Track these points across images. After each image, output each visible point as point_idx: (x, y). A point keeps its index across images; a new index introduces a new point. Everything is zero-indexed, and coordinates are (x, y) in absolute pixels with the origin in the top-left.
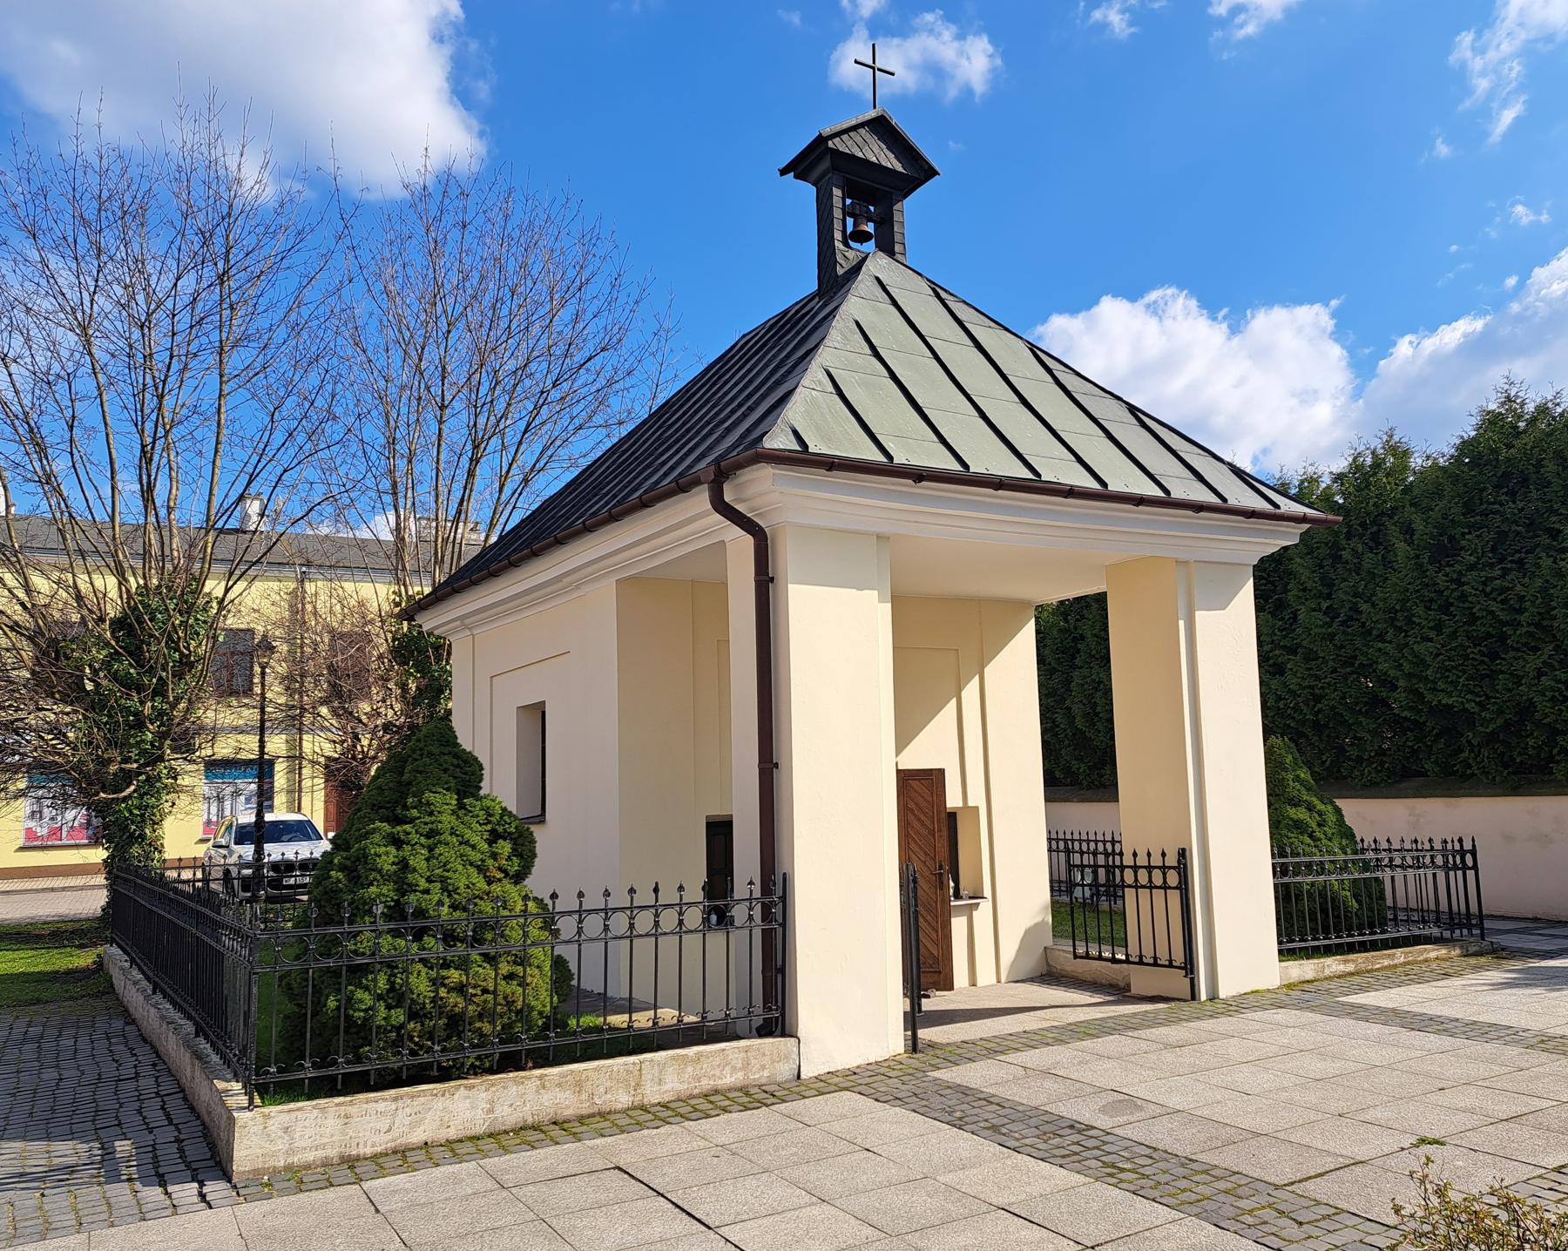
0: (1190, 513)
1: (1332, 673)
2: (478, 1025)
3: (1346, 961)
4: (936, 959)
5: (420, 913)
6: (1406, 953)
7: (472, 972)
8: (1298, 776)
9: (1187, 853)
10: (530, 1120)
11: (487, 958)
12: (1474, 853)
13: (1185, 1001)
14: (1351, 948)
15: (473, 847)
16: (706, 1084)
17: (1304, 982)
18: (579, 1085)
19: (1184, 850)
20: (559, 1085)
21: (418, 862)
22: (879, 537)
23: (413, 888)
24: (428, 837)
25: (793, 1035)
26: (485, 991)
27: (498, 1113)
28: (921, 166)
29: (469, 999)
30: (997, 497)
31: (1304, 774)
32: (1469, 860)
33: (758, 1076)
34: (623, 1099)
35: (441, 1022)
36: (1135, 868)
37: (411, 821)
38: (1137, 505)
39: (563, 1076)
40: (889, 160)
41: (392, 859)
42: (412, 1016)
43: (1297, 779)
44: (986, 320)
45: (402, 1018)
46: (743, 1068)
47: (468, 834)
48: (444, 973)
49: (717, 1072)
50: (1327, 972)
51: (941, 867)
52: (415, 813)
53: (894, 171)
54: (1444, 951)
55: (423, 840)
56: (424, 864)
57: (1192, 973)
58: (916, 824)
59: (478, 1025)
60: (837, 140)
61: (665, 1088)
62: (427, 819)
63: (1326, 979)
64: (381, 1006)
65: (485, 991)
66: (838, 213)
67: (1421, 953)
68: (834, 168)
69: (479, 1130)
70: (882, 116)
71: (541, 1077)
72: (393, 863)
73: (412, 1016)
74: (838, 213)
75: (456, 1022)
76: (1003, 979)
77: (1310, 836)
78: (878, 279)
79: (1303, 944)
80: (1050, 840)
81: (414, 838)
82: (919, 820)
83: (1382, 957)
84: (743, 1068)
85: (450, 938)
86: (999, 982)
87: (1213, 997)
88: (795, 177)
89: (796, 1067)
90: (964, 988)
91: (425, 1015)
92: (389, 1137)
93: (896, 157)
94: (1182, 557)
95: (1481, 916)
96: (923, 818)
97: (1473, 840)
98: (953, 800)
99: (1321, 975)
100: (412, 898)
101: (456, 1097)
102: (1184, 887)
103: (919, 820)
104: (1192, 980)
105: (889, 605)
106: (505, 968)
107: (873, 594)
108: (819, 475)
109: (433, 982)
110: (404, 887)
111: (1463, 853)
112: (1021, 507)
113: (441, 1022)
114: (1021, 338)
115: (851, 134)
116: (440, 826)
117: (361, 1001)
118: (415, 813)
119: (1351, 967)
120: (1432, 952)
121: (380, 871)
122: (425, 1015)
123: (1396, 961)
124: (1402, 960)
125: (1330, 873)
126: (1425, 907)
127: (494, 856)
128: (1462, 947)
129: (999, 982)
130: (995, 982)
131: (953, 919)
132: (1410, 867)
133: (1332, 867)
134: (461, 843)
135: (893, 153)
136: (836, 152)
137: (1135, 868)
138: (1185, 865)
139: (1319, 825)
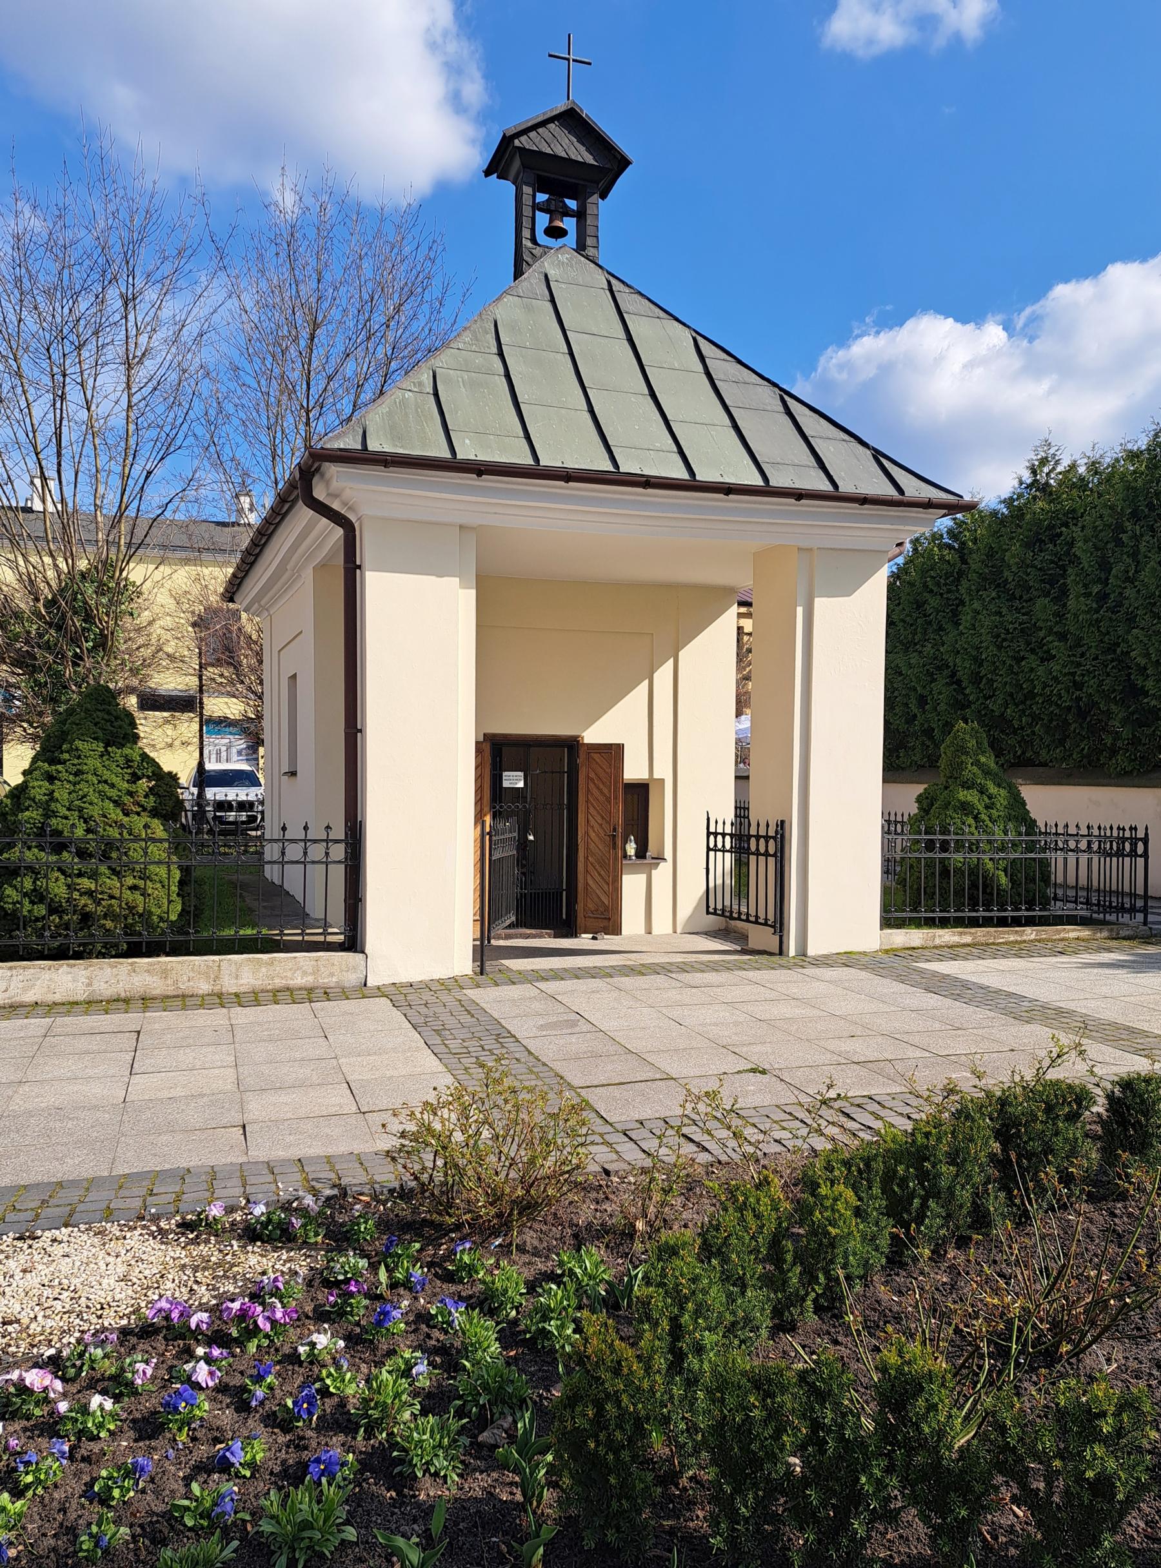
0: (721, 496)
1: (1094, 659)
2: (102, 922)
3: (961, 934)
4: (607, 909)
5: (58, 833)
6: (1038, 931)
7: (100, 882)
8: (979, 761)
9: (787, 825)
10: (123, 995)
11: (114, 872)
12: (1145, 840)
13: (771, 954)
14: (974, 923)
15: (113, 786)
16: (279, 983)
17: (908, 949)
18: (165, 973)
19: (783, 822)
20: (148, 971)
21: (62, 793)
22: (461, 527)
23: (54, 814)
24: (76, 775)
25: (363, 952)
26: (112, 897)
27: (95, 987)
28: (615, 156)
29: (98, 903)
30: (567, 488)
31: (985, 759)
32: (1140, 848)
33: (325, 980)
34: (204, 987)
35: (75, 918)
36: (758, 837)
37: (64, 762)
38: (727, 494)
39: (150, 964)
40: (579, 153)
41: (43, 791)
42: (52, 910)
43: (977, 763)
44: (657, 310)
45: (44, 912)
46: (314, 973)
47: (107, 775)
48: (79, 881)
49: (289, 974)
50: (937, 942)
51: (615, 830)
52: (66, 756)
53: (584, 164)
54: (1087, 933)
55: (71, 778)
56: (66, 796)
57: (781, 931)
58: (595, 791)
59: (102, 922)
60: (524, 138)
61: (242, 982)
62: (76, 761)
63: (935, 947)
64: (26, 902)
65: (112, 897)
66: (527, 211)
67: (1059, 932)
68: (524, 166)
69: (81, 997)
70: (572, 109)
71: (132, 964)
72: (45, 795)
73: (52, 910)
74: (527, 211)
75: (86, 918)
76: (679, 930)
77: (976, 818)
78: (546, 276)
79: (915, 915)
80: (736, 808)
81: (64, 775)
82: (598, 788)
83: (1004, 933)
84: (314, 973)
85: (82, 854)
86: (675, 932)
87: (802, 953)
88: (498, 177)
89: (363, 977)
90: (639, 936)
91: (63, 911)
92: (7, 995)
93: (588, 150)
94: (801, 544)
95: (1146, 897)
96: (601, 786)
97: (1147, 828)
98: (634, 770)
99: (931, 944)
100: (53, 821)
101: (60, 971)
102: (781, 857)
103: (598, 788)
104: (781, 937)
105: (474, 592)
106: (130, 881)
107: (452, 582)
108: (378, 472)
109: (69, 886)
110: (49, 813)
111: (1134, 841)
112: (556, 493)
113: (75, 918)
114: (688, 327)
115: (540, 130)
116: (85, 767)
117: (9, 896)
118: (66, 756)
119: (967, 939)
120: (1073, 932)
121: (33, 800)
122: (63, 911)
123: (1025, 938)
124: (1033, 937)
125: (984, 852)
126: (1083, 881)
127: (130, 794)
128: (1111, 930)
129: (675, 932)
130: (670, 931)
131: (624, 877)
132: (1061, 849)
133: (987, 848)
134: (99, 782)
135: (583, 145)
136: (522, 150)
137: (758, 837)
138: (783, 836)
139: (987, 807)
